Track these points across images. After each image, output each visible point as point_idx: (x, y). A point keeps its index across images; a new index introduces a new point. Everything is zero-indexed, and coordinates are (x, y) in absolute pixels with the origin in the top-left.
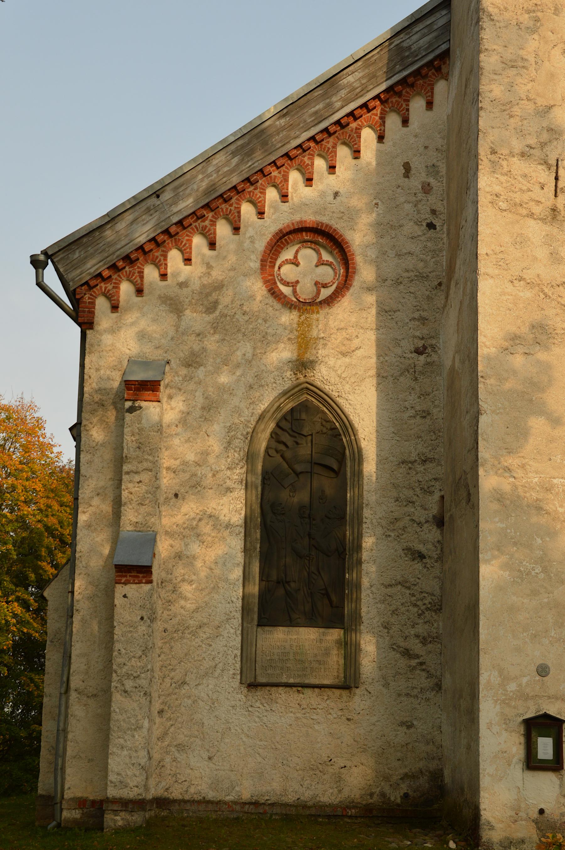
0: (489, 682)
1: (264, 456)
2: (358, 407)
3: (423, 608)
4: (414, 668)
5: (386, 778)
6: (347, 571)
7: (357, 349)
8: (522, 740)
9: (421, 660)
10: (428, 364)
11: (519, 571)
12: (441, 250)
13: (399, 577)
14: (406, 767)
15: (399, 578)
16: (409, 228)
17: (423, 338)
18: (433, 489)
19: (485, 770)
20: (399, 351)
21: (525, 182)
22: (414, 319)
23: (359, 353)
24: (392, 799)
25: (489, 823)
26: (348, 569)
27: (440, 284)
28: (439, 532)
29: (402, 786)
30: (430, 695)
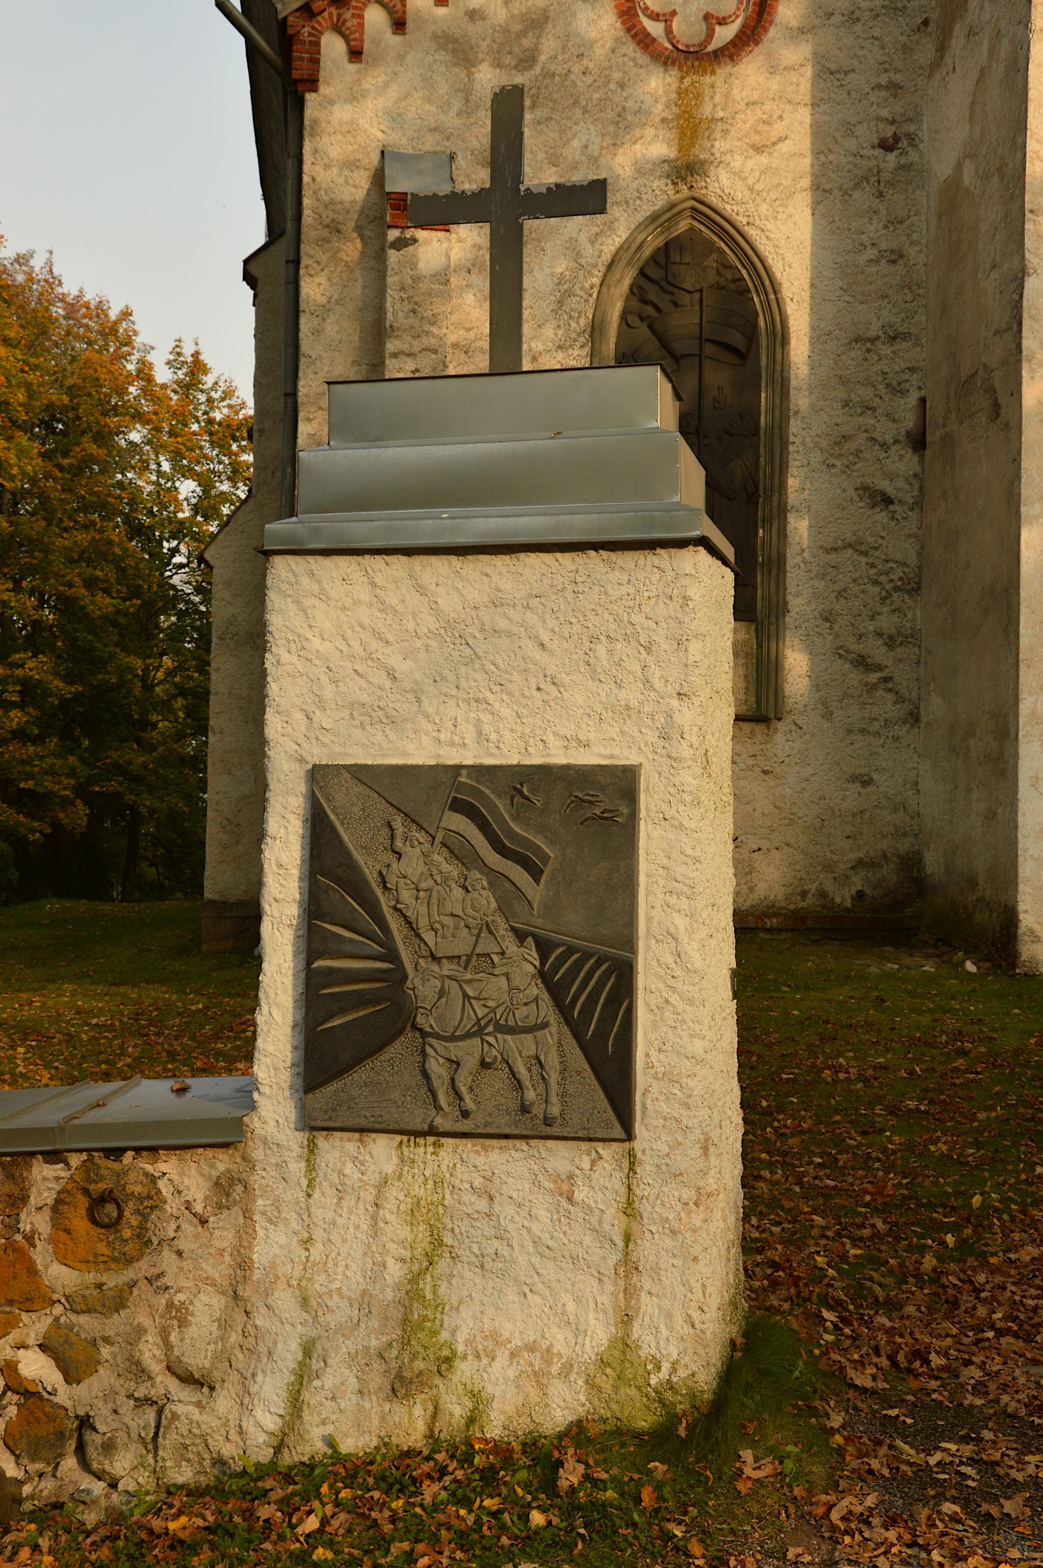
1: (620, 326)
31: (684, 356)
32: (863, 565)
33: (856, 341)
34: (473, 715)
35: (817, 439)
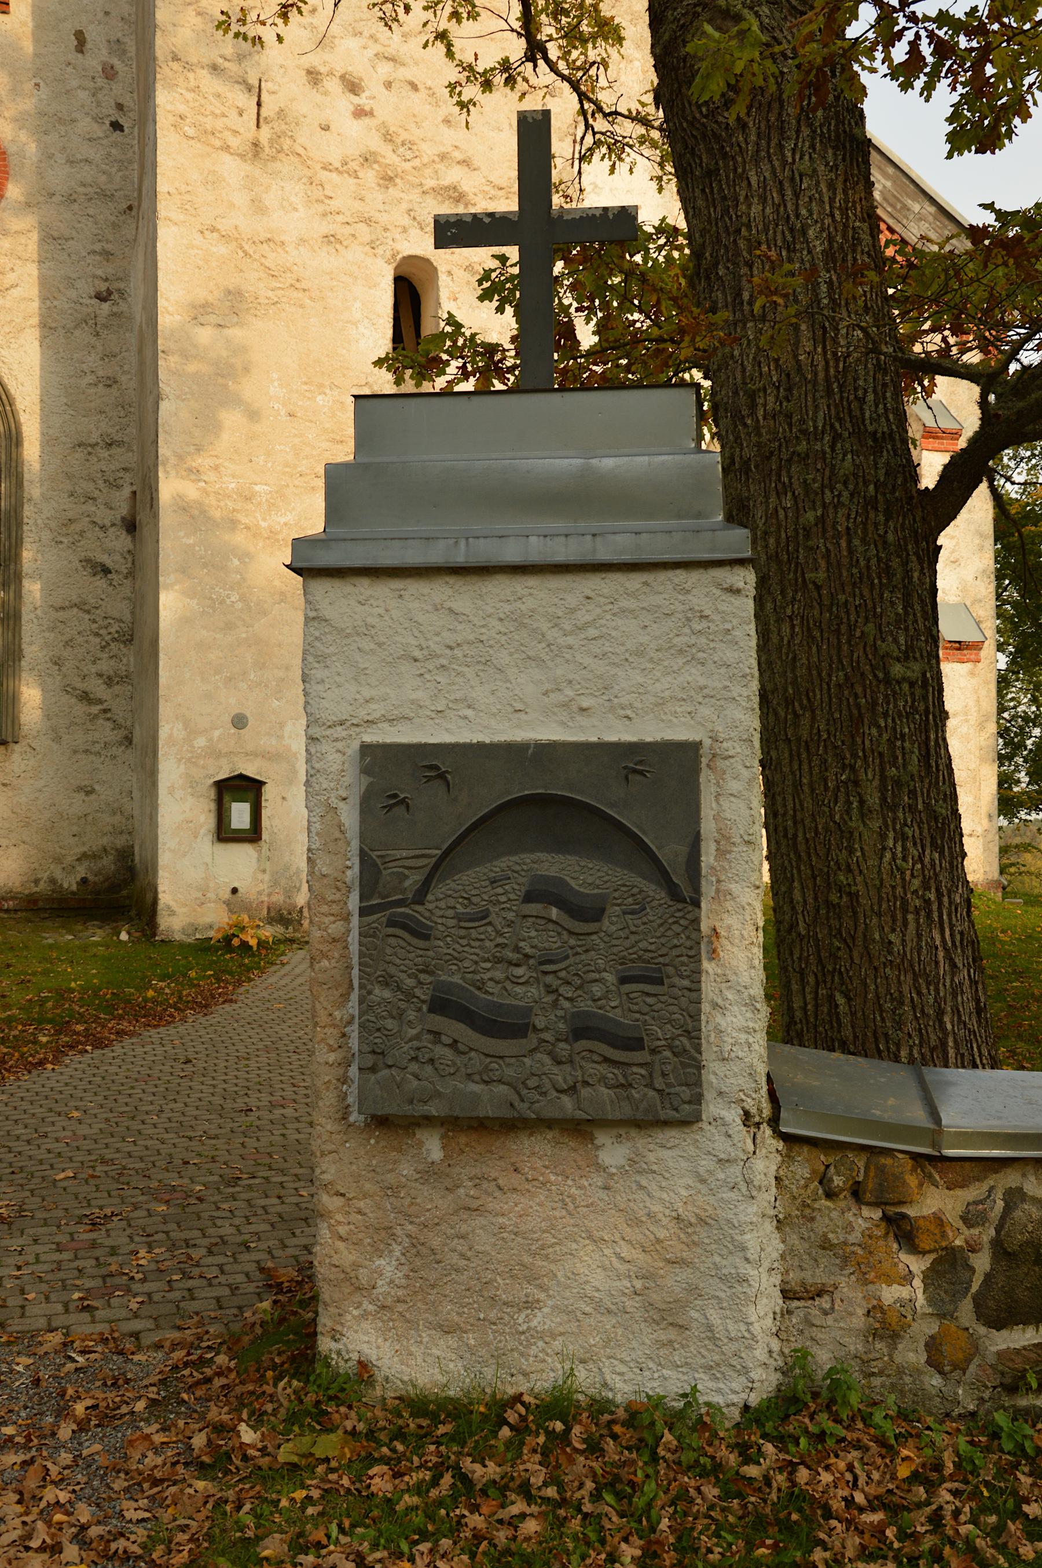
0: (171, 736)
2: (15, 366)
3: (108, 638)
4: (96, 717)
5: (58, 860)
7: (12, 286)
8: (213, 806)
9: (105, 706)
10: (114, 314)
11: (211, 598)
12: (130, 162)
13: (74, 597)
14: (84, 844)
15: (75, 599)
16: (85, 125)
17: (106, 280)
18: (121, 482)
19: (165, 844)
20: (72, 294)
21: (218, 105)
22: (94, 252)
23: (15, 292)
24: (66, 886)
25: (169, 907)
27: (130, 208)
28: (129, 538)
29: (79, 868)
30: (118, 751)
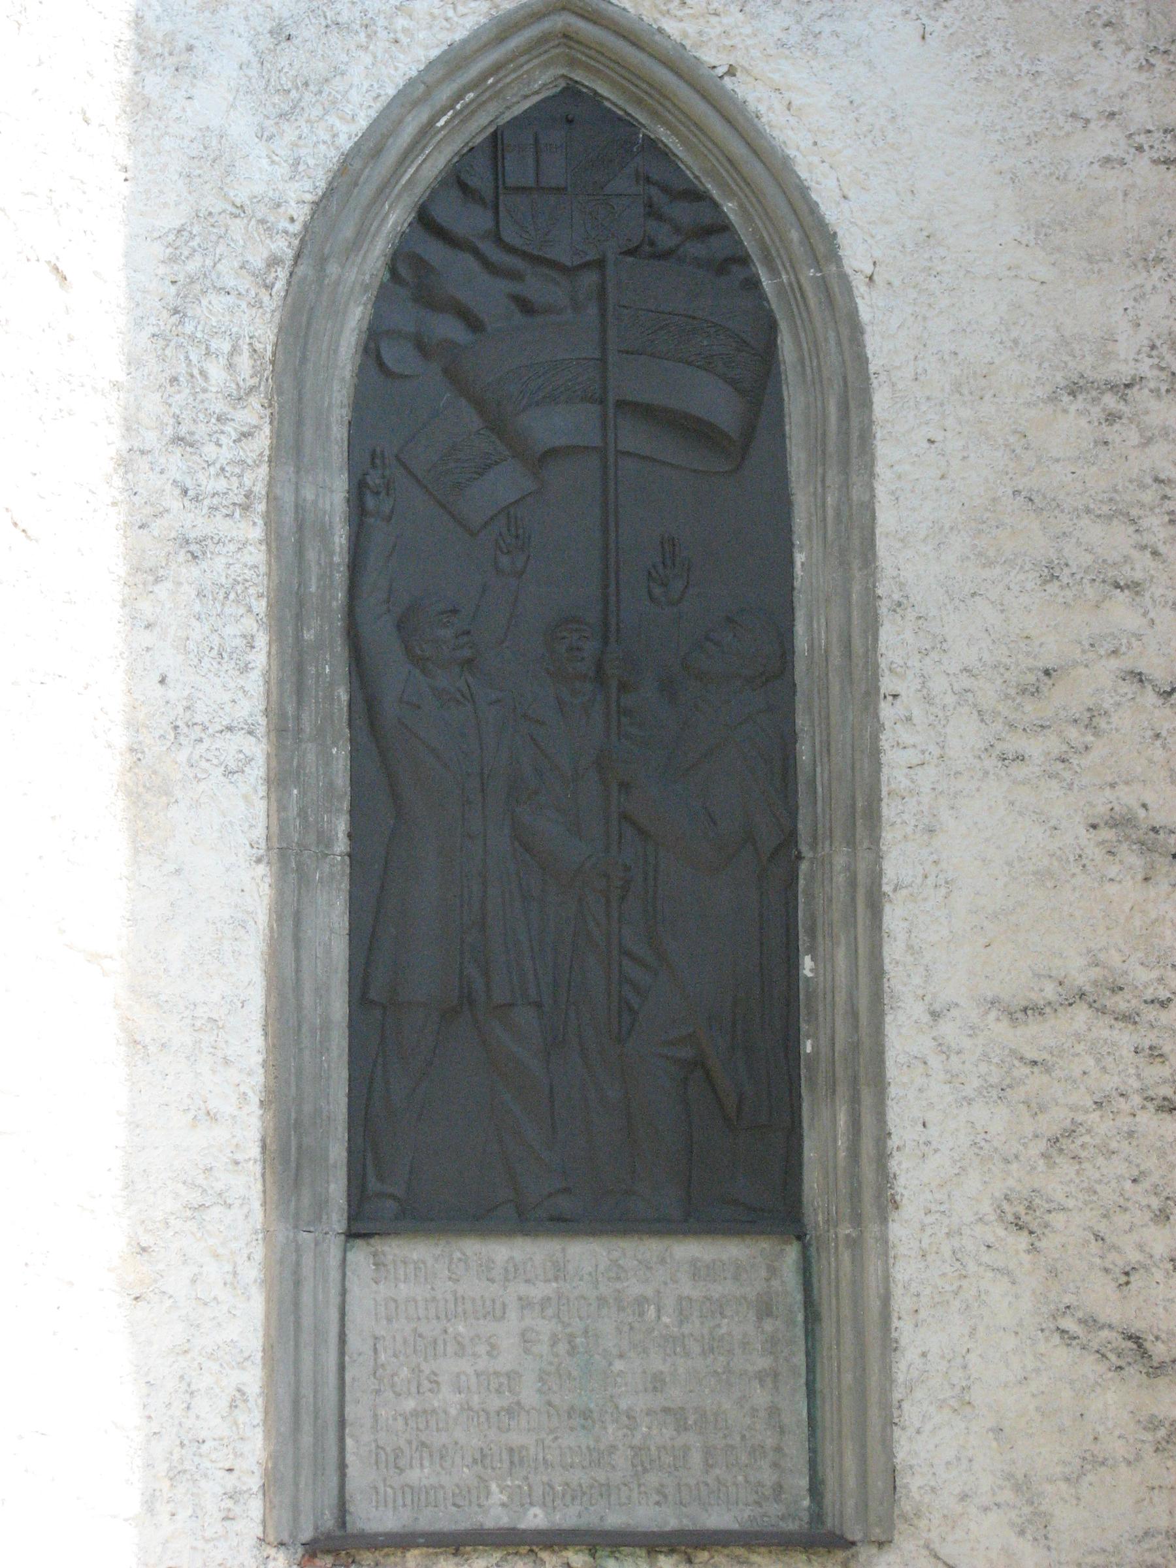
6: (803, 938)
26: (812, 932)
31: (552, 453)
32: (1127, 1053)
33: (1074, 390)
34: (744, 1458)
35: (965, 682)
